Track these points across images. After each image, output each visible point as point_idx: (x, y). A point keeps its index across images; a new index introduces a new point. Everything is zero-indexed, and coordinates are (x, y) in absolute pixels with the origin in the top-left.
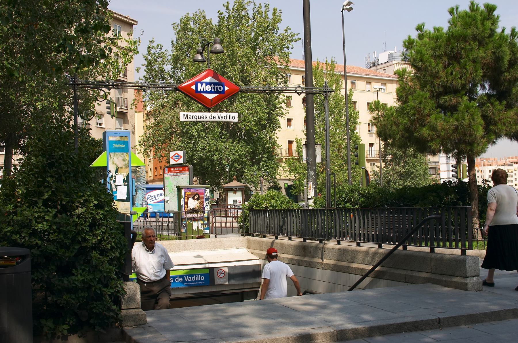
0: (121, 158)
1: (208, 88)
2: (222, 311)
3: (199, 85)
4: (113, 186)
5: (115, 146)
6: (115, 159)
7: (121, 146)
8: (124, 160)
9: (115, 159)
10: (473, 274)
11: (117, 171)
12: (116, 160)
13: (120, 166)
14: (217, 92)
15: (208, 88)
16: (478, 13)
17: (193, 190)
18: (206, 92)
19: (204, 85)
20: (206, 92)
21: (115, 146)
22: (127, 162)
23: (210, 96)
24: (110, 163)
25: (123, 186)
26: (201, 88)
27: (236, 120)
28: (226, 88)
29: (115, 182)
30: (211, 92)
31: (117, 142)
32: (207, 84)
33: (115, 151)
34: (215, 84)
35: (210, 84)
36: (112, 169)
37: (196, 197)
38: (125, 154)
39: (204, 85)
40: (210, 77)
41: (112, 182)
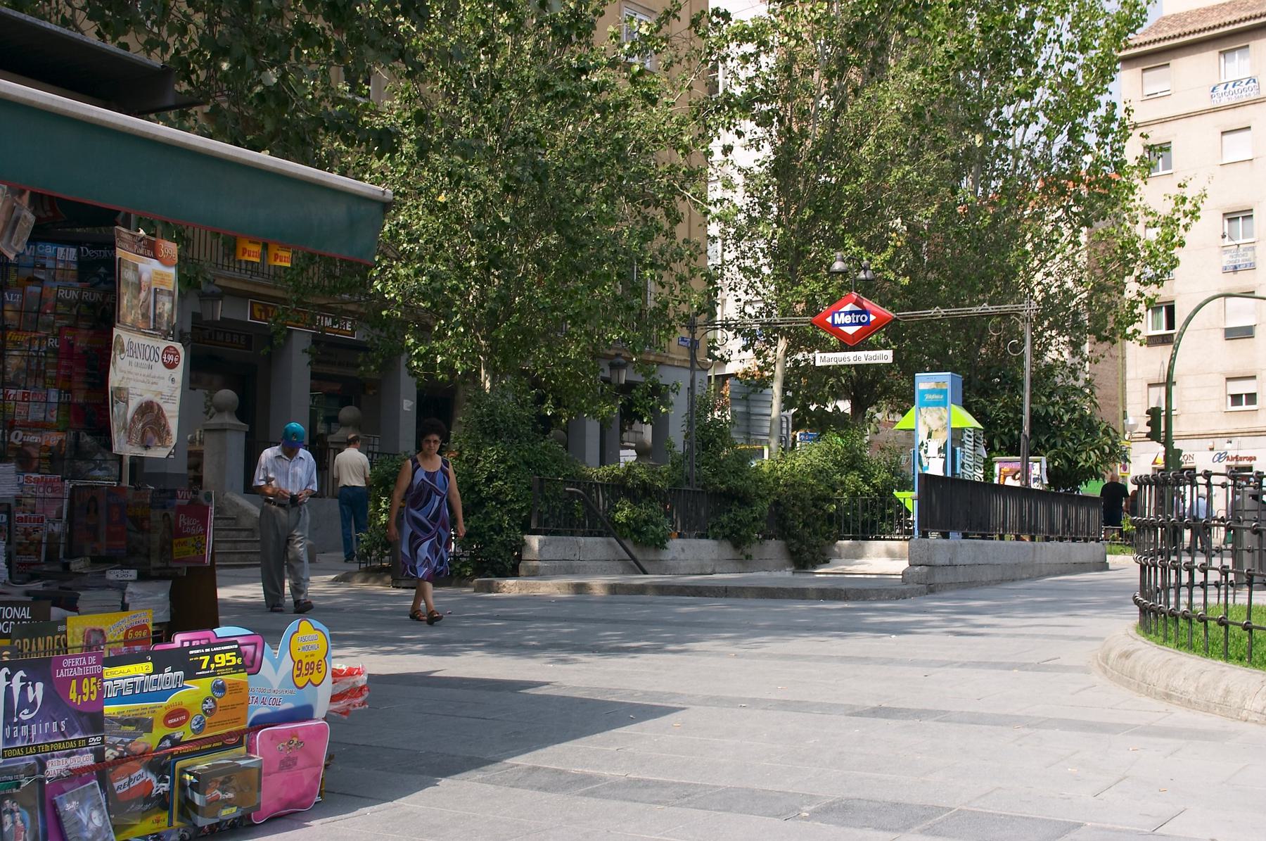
0: (936, 416)
1: (848, 319)
2: (533, 586)
3: (836, 315)
4: (924, 459)
5: (928, 397)
6: (928, 416)
7: (937, 397)
8: (941, 419)
9: (928, 416)
10: (918, 563)
11: (930, 436)
12: (929, 419)
13: (934, 428)
14: (860, 323)
15: (848, 319)
16: (646, 280)
17: (1014, 464)
18: (845, 325)
19: (842, 315)
20: (845, 325)
21: (928, 397)
22: (945, 421)
23: (850, 330)
24: (920, 423)
25: (938, 459)
26: (838, 320)
27: (890, 360)
28: (872, 318)
29: (926, 452)
30: (851, 324)
31: (931, 391)
32: (846, 313)
33: (928, 405)
34: (856, 313)
35: (850, 313)
36: (922, 436)
37: (1017, 476)
38: (942, 409)
39: (842, 315)
40: (851, 304)
41: (922, 452)
